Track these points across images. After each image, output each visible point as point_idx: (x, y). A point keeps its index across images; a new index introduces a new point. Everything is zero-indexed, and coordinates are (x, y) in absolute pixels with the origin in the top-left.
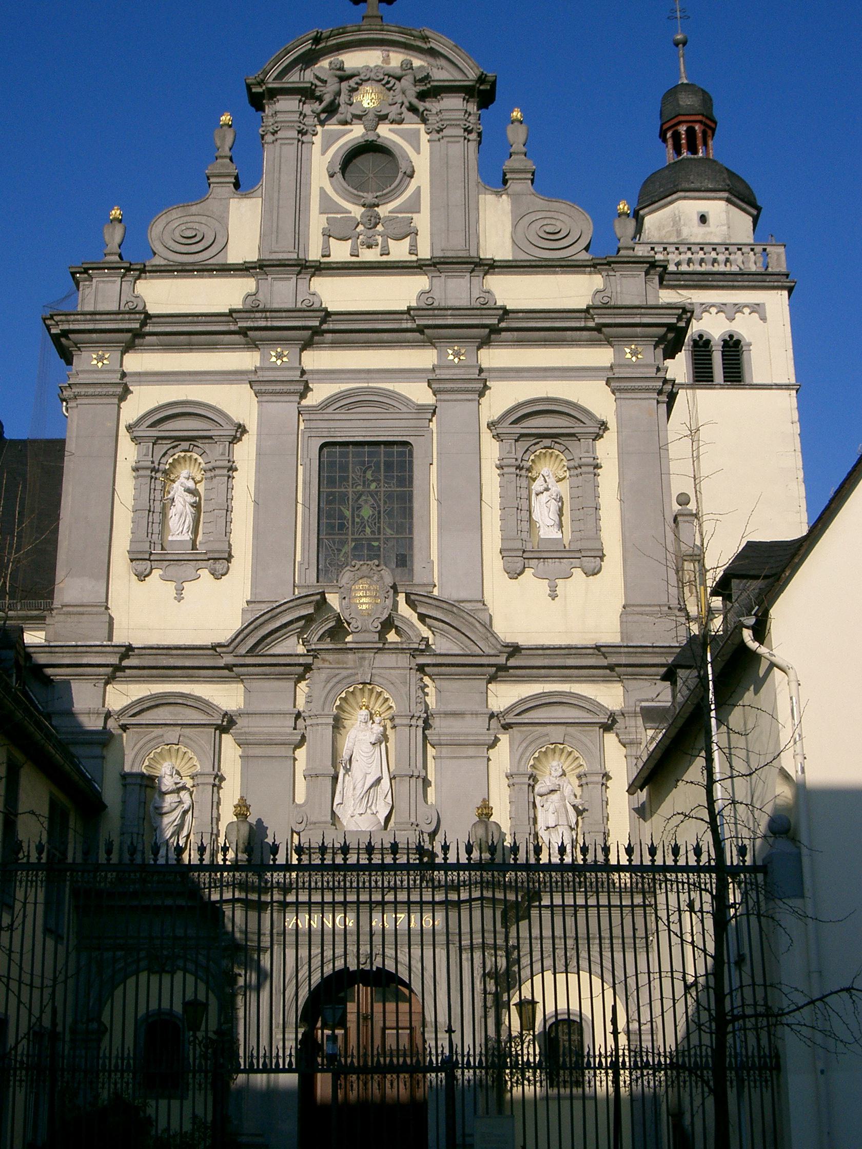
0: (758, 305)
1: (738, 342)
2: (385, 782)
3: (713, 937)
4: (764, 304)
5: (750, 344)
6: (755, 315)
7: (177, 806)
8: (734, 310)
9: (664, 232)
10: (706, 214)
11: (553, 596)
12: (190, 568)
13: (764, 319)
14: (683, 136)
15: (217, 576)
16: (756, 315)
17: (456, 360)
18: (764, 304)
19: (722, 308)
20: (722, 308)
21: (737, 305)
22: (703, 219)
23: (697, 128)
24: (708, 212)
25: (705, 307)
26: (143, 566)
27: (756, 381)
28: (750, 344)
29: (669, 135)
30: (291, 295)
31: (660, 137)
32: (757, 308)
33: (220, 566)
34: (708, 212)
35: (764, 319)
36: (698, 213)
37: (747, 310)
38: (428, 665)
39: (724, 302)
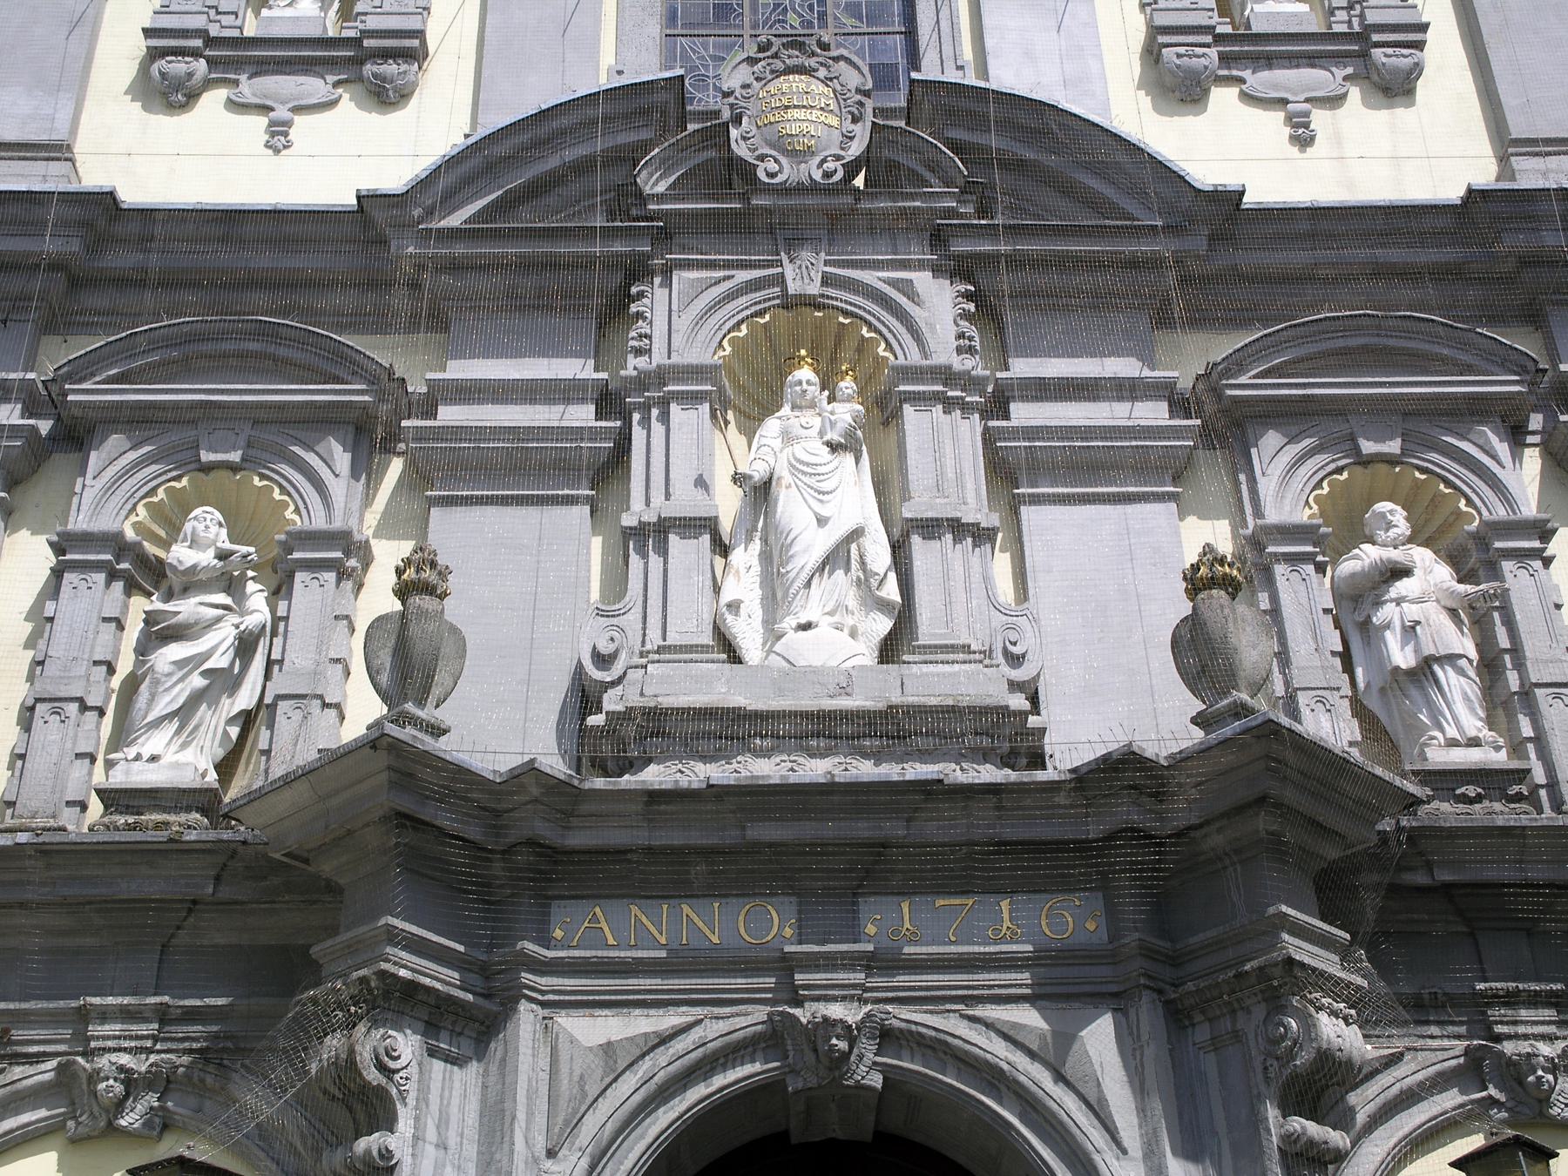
2: (878, 553)
7: (219, 620)
11: (1303, 139)
12: (314, 87)
15: (386, 97)
26: (178, 66)
33: (390, 68)
38: (991, 259)
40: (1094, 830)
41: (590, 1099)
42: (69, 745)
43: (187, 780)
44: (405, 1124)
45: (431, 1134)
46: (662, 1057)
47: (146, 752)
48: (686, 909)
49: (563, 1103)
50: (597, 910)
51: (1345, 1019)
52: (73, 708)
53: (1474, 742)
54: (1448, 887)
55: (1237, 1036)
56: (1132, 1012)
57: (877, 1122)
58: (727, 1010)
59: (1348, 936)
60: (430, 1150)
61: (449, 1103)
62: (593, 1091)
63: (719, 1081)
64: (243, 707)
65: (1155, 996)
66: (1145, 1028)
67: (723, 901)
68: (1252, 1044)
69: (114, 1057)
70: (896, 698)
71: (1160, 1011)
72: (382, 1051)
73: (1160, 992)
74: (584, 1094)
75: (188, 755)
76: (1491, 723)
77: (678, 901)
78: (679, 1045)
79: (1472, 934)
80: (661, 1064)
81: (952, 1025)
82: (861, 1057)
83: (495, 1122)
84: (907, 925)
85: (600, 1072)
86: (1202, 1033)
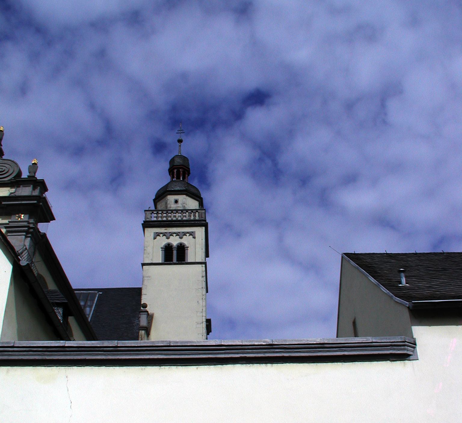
0: (192, 232)
1: (184, 246)
3: (62, 315)
4: (195, 232)
5: (188, 247)
6: (191, 236)
8: (183, 234)
9: (162, 208)
10: (177, 200)
13: (194, 238)
14: (175, 173)
16: (178, 237)
17: (19, 219)
18: (195, 232)
19: (177, 234)
20: (177, 234)
21: (171, 232)
22: (176, 202)
23: (181, 170)
24: (178, 199)
25: (172, 234)
27: (189, 261)
28: (188, 247)
29: (171, 173)
30: (10, 159)
31: (170, 172)
32: (192, 234)
34: (178, 199)
35: (194, 238)
36: (174, 199)
37: (188, 235)
39: (192, 231)
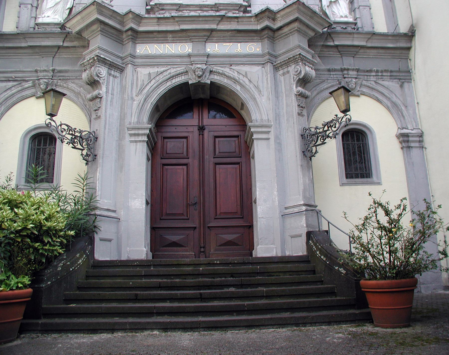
40: (259, 27)
41: (145, 85)
42: (29, 15)
43: (56, 21)
44: (104, 89)
45: (110, 92)
46: (161, 76)
47: (46, 15)
48: (167, 46)
49: (139, 86)
50: (147, 46)
51: (311, 68)
52: (29, 6)
53: (346, 17)
54: (337, 46)
55: (288, 72)
56: (266, 67)
57: (210, 94)
58: (176, 66)
59: (314, 52)
60: (110, 95)
61: (114, 86)
62: (145, 84)
63: (174, 81)
64: (69, 7)
65: (271, 64)
66: (268, 70)
67: (176, 44)
68: (291, 73)
69: (43, 80)
70: (217, 2)
71: (272, 67)
72: (98, 73)
73: (272, 63)
74: (144, 84)
75: (57, 17)
76: (350, 13)
77: (165, 44)
78: (165, 74)
79: (342, 57)
80: (161, 78)
81: (227, 70)
82: (205, 76)
83: (65, 5)
84: (217, 49)
85: (147, 79)
86: (281, 72)
